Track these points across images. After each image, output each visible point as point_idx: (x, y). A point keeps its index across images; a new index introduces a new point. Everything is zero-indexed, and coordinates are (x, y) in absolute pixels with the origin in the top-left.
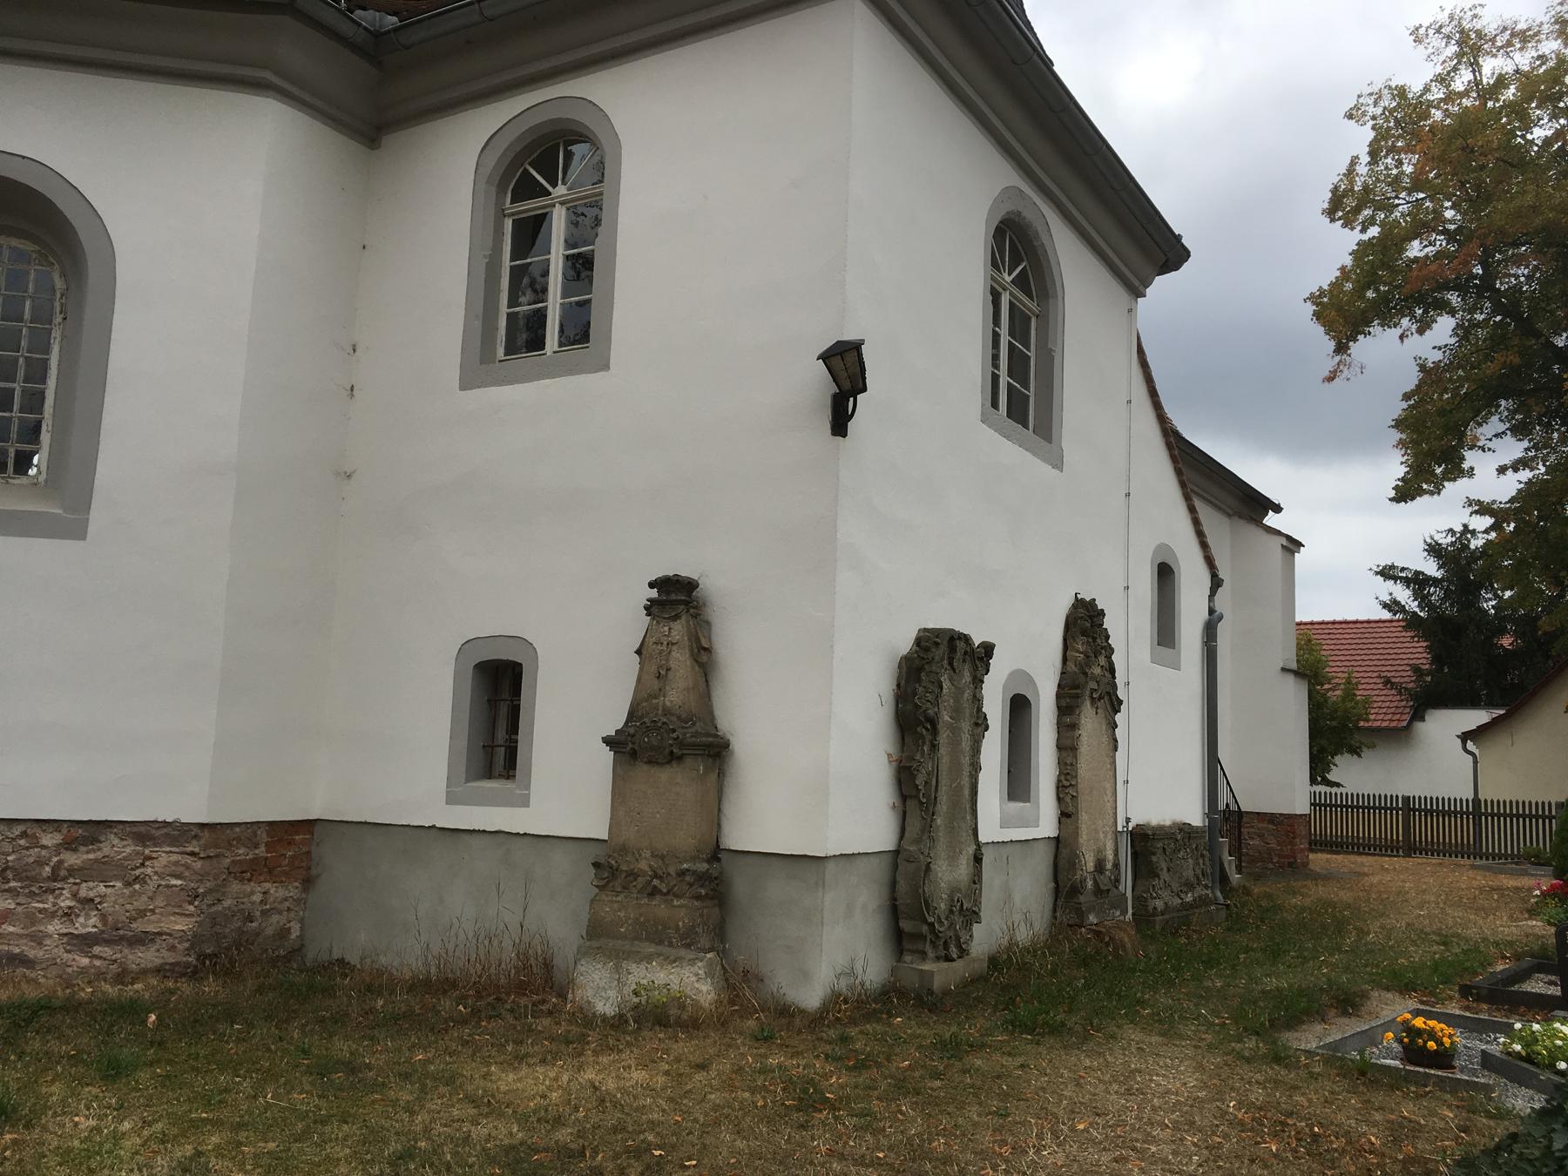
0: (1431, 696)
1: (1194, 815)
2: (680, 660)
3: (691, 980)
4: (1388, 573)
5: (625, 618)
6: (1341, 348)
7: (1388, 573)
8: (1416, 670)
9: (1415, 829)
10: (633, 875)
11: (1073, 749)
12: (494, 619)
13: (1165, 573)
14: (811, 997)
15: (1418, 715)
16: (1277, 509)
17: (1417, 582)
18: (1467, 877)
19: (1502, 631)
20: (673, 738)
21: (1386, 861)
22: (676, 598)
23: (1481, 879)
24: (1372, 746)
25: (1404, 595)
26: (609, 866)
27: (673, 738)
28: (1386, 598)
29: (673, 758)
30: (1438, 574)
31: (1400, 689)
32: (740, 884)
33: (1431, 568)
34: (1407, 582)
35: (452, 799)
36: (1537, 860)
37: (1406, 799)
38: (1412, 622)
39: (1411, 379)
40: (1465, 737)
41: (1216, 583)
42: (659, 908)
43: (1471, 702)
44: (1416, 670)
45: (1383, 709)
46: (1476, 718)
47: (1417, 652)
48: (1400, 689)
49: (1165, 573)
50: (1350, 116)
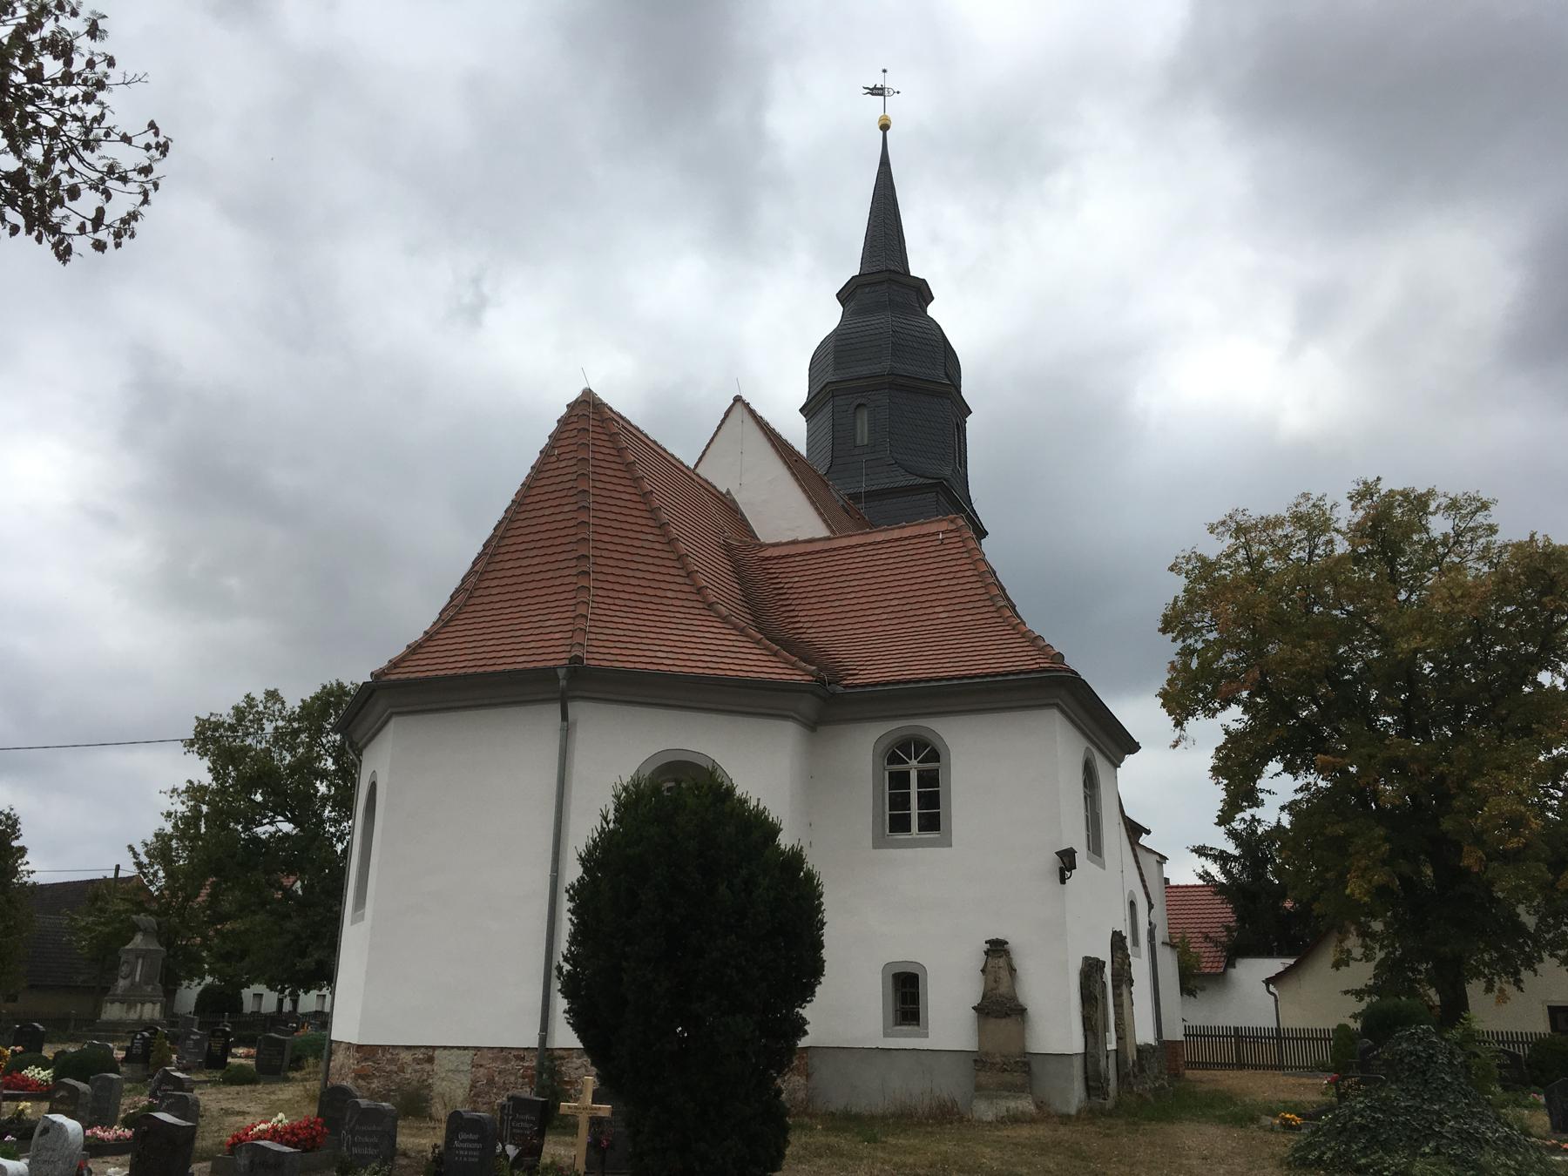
0: (1239, 948)
1: (1152, 1041)
2: (1004, 974)
3: (1025, 1104)
4: (1201, 851)
5: (972, 956)
6: (1179, 724)
7: (1201, 851)
8: (1228, 928)
9: (1243, 1048)
10: (993, 1064)
11: (1121, 1005)
12: (904, 953)
13: (1132, 904)
14: (1073, 1111)
15: (1230, 964)
16: (1148, 832)
17: (1222, 858)
18: (1281, 1079)
19: (1284, 897)
20: (1000, 1006)
21: (1231, 1073)
22: (997, 948)
23: (1292, 1080)
24: (1203, 989)
25: (1214, 869)
26: (979, 1061)
27: (1000, 1006)
28: (1200, 871)
29: (1007, 1015)
30: (1236, 852)
31: (1216, 943)
32: (1035, 1067)
33: (1231, 848)
34: (1215, 858)
35: (886, 1035)
36: (1321, 1068)
37: (1236, 1029)
38: (1219, 889)
39: (1221, 739)
40: (1268, 982)
41: (1151, 906)
42: (1007, 1077)
43: (1268, 953)
44: (1228, 928)
45: (1209, 959)
46: (1275, 966)
47: (1224, 913)
48: (1216, 943)
49: (1132, 904)
50: (1171, 569)
